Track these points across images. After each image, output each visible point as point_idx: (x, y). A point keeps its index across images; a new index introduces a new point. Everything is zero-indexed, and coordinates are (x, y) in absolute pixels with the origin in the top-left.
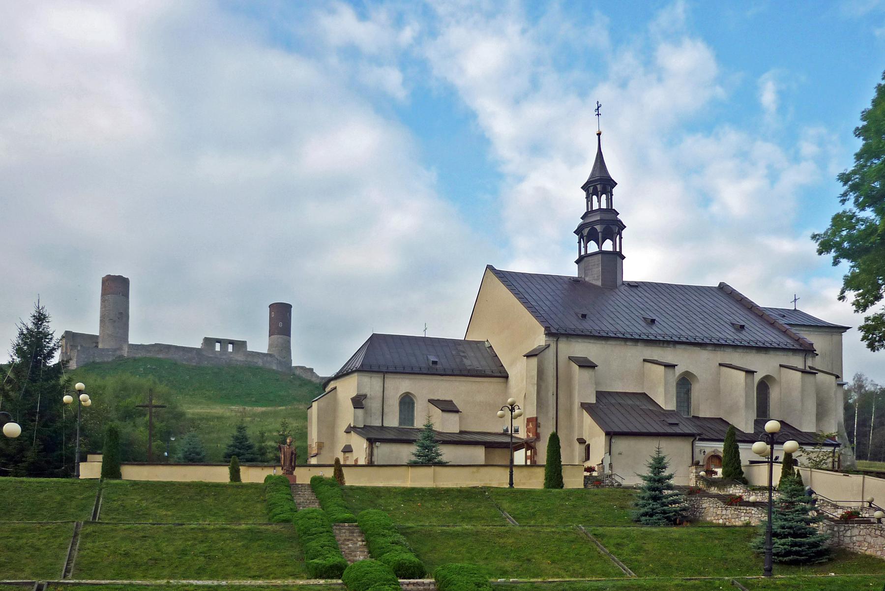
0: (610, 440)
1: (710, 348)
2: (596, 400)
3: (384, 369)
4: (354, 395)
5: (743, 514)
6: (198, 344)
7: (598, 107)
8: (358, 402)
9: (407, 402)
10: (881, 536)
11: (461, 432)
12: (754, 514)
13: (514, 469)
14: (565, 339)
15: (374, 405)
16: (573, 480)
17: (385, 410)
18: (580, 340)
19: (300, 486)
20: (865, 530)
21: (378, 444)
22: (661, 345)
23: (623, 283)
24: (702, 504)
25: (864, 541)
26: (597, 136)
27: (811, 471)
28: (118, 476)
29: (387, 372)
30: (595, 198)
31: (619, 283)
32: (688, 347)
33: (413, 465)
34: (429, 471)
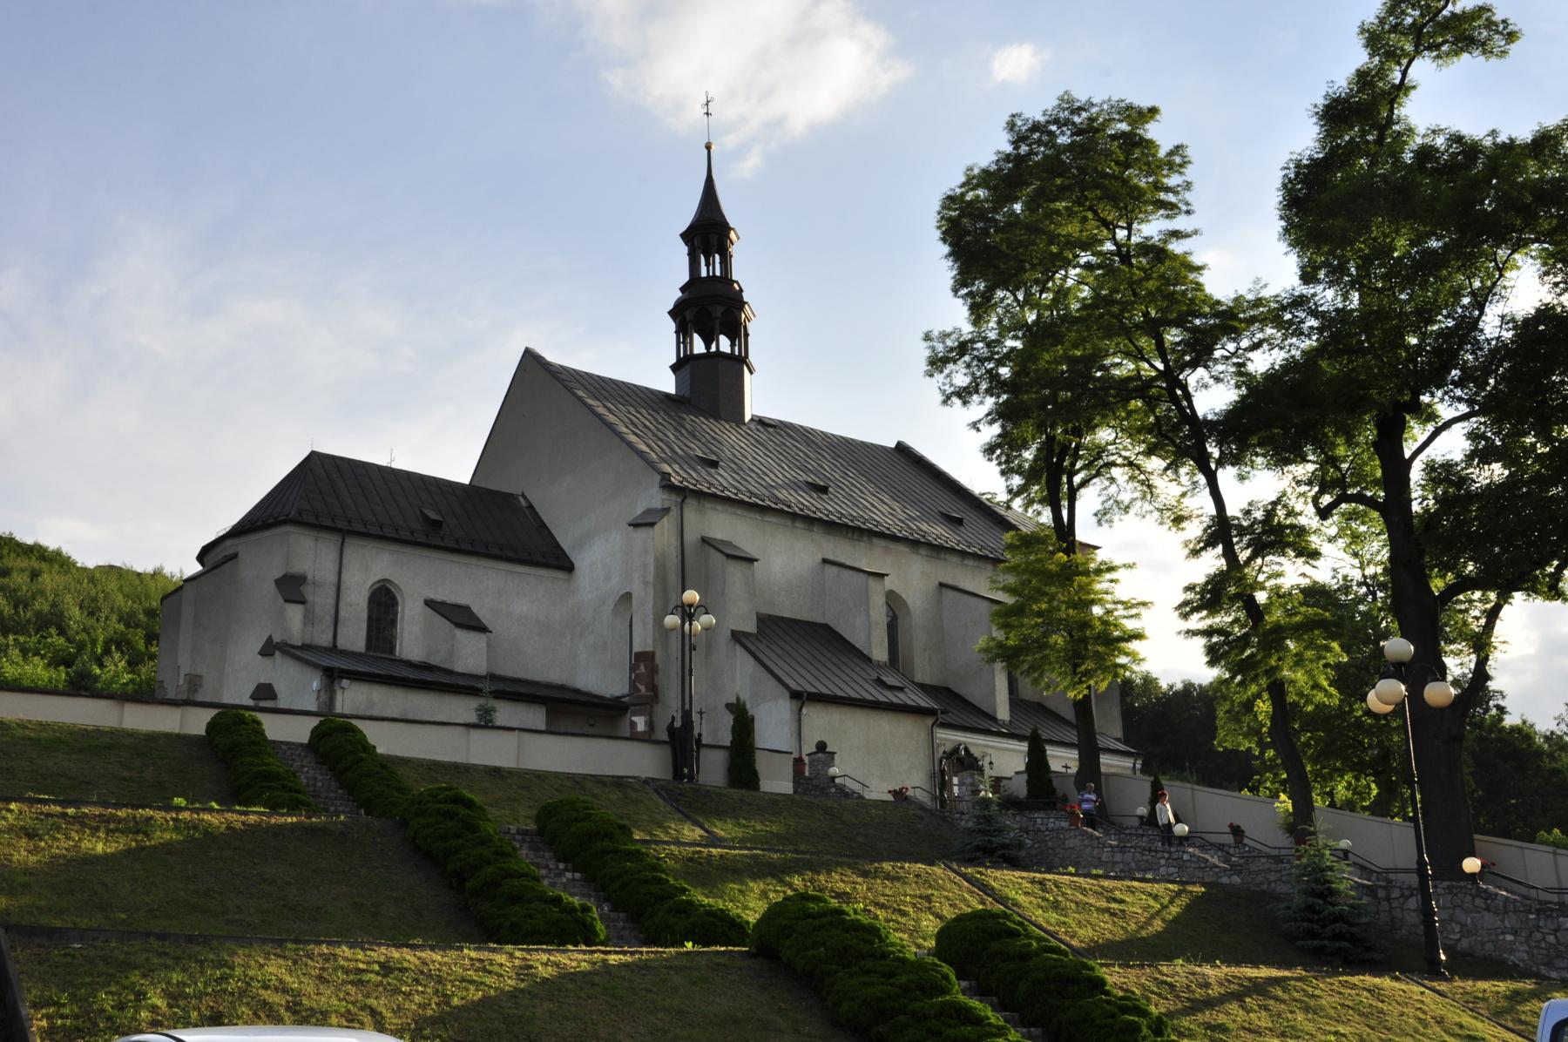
0: (800, 710)
1: (923, 551)
2: (758, 627)
4: (278, 575)
5: (1163, 862)
7: (707, 104)
9: (383, 602)
10: (1487, 909)
12: (1189, 861)
15: (322, 600)
17: (342, 613)
18: (719, 507)
19: (284, 747)
20: (1450, 897)
21: (345, 683)
24: (1065, 839)
25: (1452, 920)
26: (706, 151)
27: (1193, 790)
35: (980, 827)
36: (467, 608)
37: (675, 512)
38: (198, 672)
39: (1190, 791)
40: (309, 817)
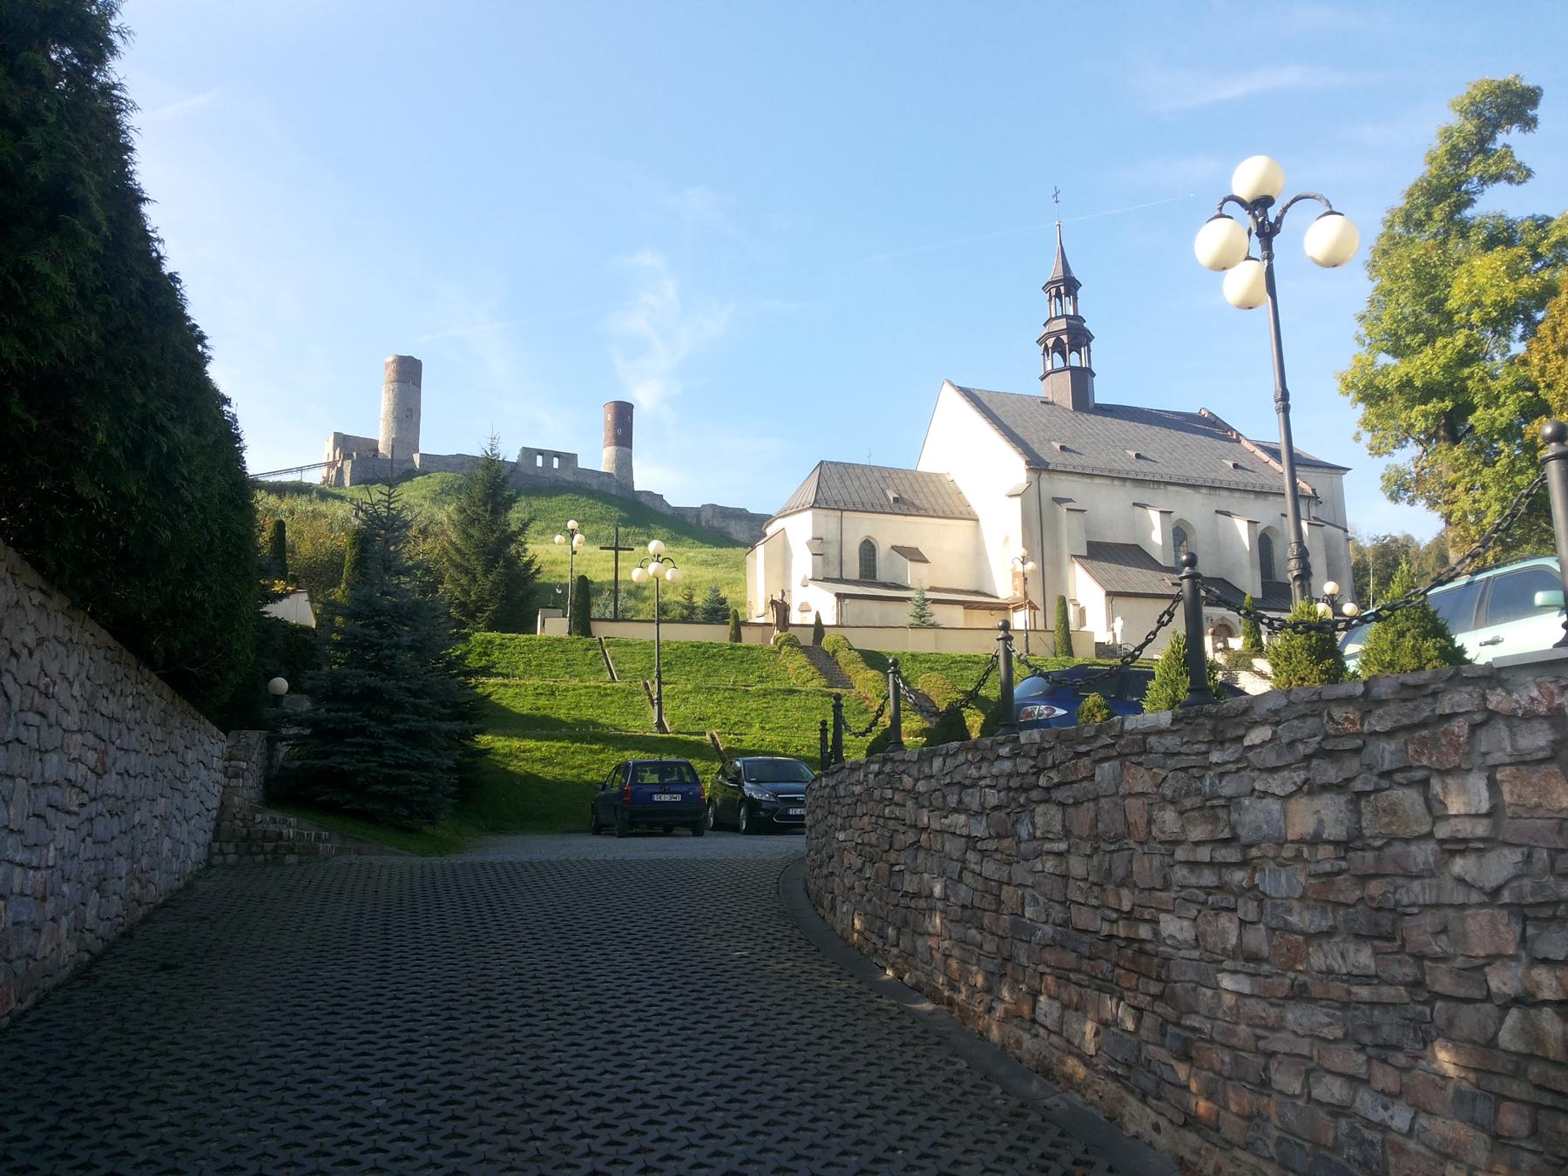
31: (1091, 405)
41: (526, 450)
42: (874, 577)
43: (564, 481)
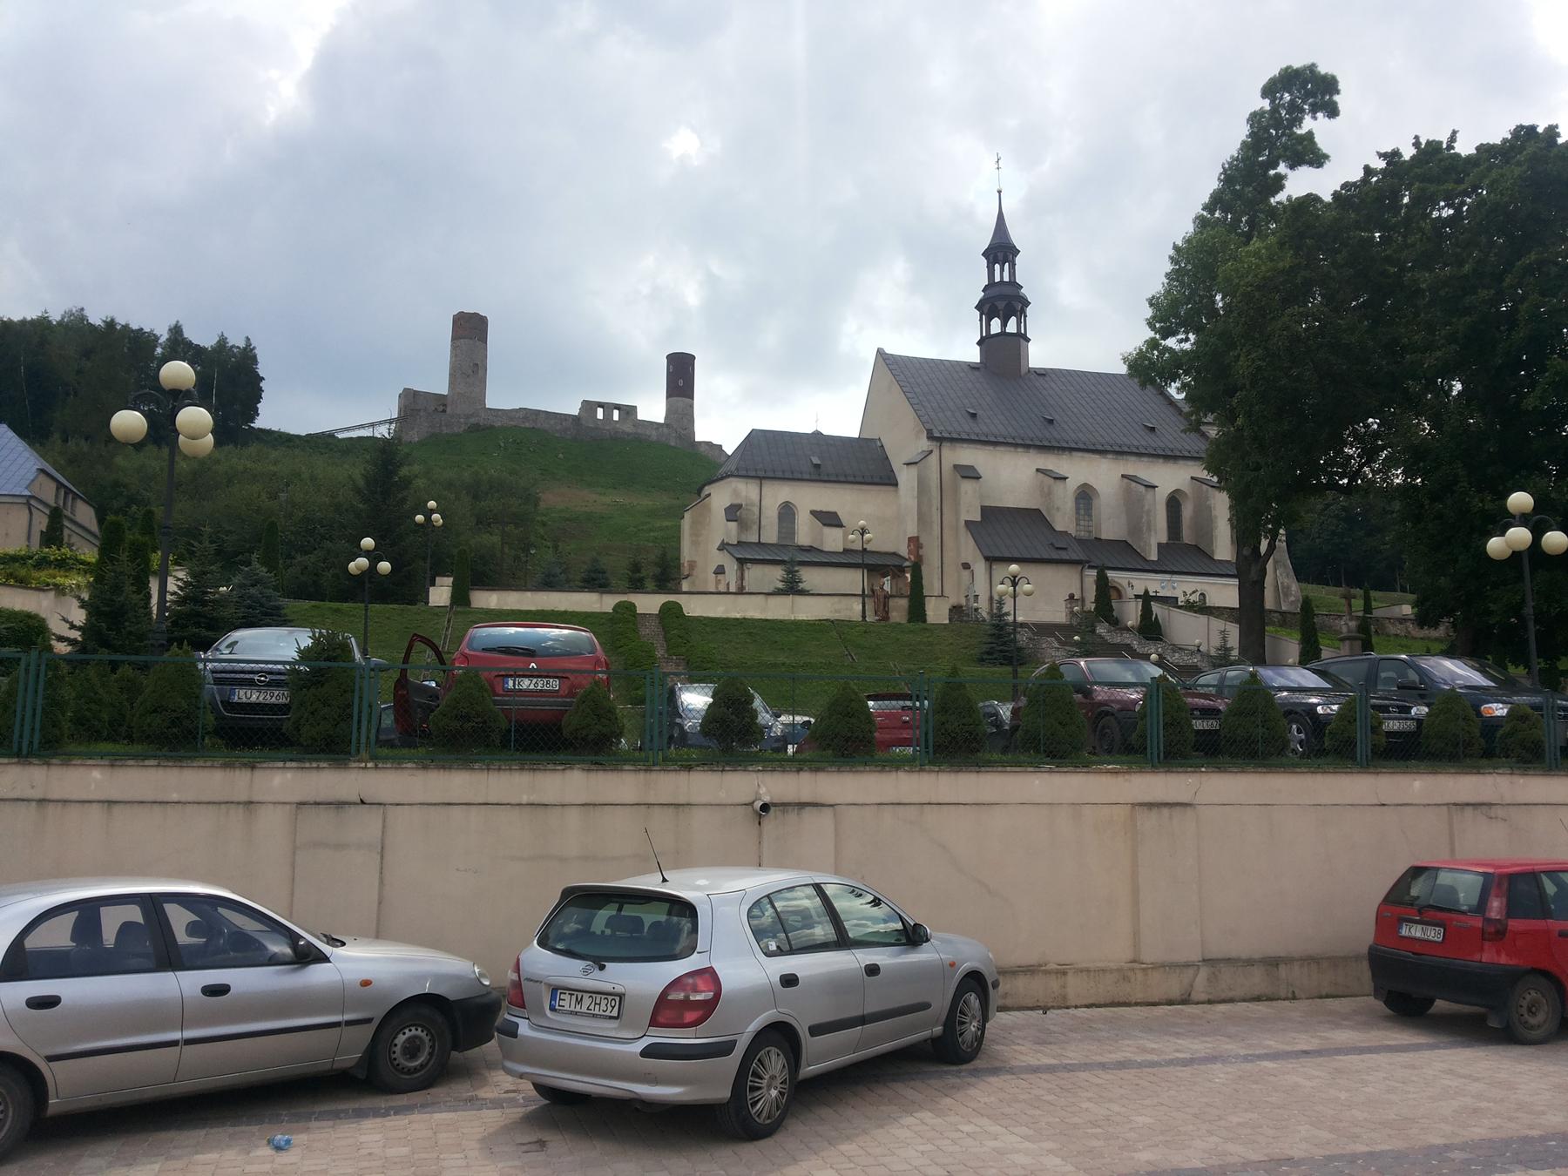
1: (1110, 456)
3: (761, 474)
6: (574, 409)
8: (733, 512)
9: (787, 512)
11: (846, 551)
13: (866, 599)
14: (949, 444)
16: (936, 612)
17: (762, 523)
18: (965, 445)
22: (1056, 452)
23: (1029, 370)
28: (467, 602)
29: (764, 478)
30: (997, 267)
31: (1024, 370)
32: (1087, 455)
33: (778, 592)
34: (788, 600)
35: (1350, 634)
36: (835, 514)
37: (936, 453)
38: (693, 559)
39: (1167, 611)
40: (109, 629)
41: (585, 403)
42: (925, 621)
43: (624, 432)
